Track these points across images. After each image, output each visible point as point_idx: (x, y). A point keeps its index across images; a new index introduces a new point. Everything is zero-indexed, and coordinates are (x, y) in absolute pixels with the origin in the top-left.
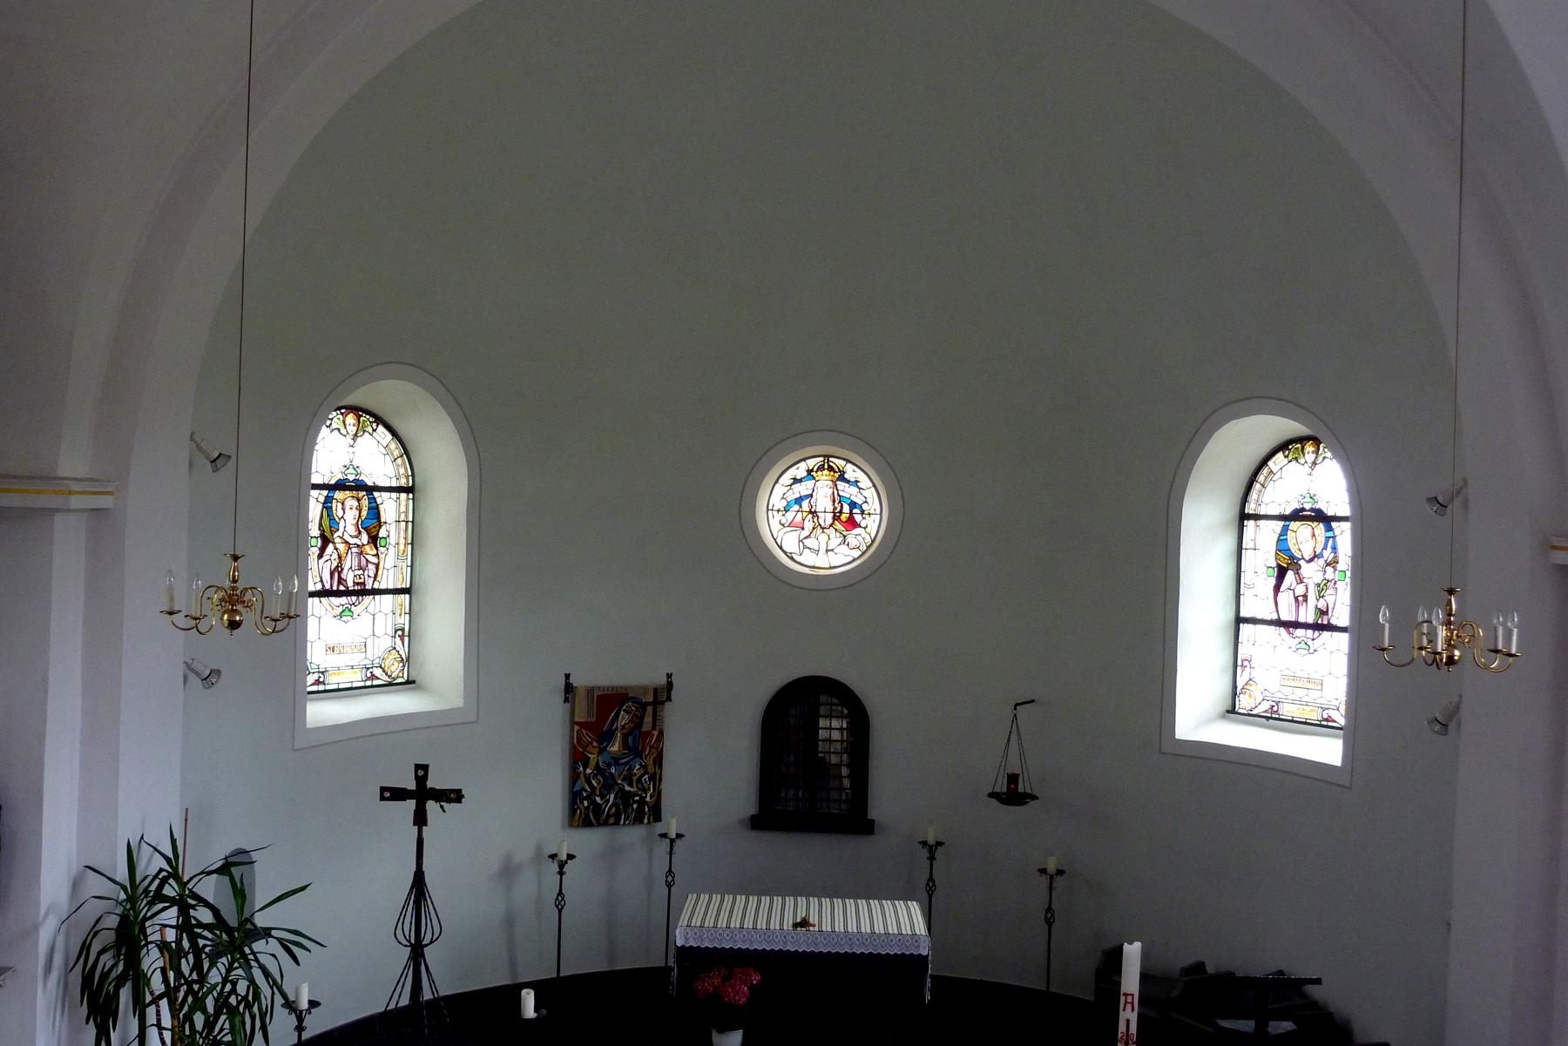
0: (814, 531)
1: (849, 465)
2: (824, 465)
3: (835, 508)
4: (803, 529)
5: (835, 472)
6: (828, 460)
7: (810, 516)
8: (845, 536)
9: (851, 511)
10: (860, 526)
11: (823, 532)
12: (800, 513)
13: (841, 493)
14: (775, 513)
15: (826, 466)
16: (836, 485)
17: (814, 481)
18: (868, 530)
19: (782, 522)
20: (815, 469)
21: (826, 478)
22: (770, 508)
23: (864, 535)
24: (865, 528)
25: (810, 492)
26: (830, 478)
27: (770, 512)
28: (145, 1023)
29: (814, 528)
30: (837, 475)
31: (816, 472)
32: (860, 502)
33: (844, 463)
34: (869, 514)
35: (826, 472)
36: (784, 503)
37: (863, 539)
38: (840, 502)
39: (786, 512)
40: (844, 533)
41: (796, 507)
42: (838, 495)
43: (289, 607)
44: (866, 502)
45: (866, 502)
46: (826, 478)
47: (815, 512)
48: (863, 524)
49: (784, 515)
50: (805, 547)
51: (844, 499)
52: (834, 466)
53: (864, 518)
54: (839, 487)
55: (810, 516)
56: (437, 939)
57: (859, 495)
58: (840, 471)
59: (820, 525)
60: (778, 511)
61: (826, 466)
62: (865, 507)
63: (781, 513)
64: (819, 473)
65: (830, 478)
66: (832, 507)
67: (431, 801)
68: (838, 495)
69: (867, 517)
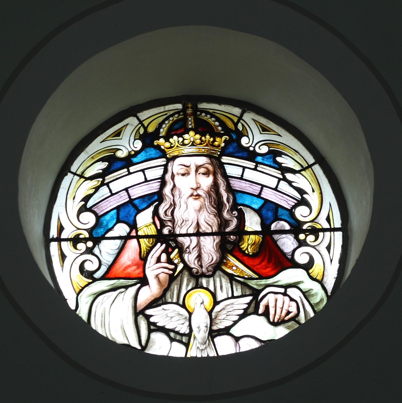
0: (175, 287)
1: (248, 117)
2: (185, 120)
3: (223, 223)
4: (144, 281)
5: (215, 134)
6: (196, 109)
7: (160, 248)
8: (255, 293)
9: (265, 225)
10: (297, 265)
11: (198, 286)
12: (133, 243)
13: (236, 184)
14: (66, 246)
15: (191, 124)
16: (222, 166)
17: (162, 161)
18: (316, 271)
19: (89, 267)
20: (163, 132)
21: (193, 150)
22: (53, 233)
23: (308, 284)
24: (308, 267)
25: (155, 187)
26: (203, 149)
27: (54, 246)
28: (171, 302)
29: (172, 278)
30: (220, 142)
31: (167, 138)
32: (287, 203)
33: (237, 111)
34: (315, 232)
35: (190, 137)
36: (89, 219)
37: (306, 294)
38: (235, 206)
39: (97, 241)
40: (253, 284)
41: (122, 229)
42: (230, 189)
43: (236, 350)
44: (303, 202)
45: (303, 202)
46: (193, 150)
47: (173, 236)
48: (301, 258)
49: (89, 251)
50: (153, 328)
51: (247, 200)
52: (212, 121)
53: (302, 243)
54: (230, 170)
55: (160, 248)
56: (277, 133)
57: (284, 186)
58: (227, 131)
59: (187, 267)
60: (76, 240)
61: (191, 124)
62: (301, 212)
63: (82, 246)
64: (175, 139)
65: (203, 149)
66: (214, 221)
67: (150, 320)
68: (230, 189)
69: (311, 238)
